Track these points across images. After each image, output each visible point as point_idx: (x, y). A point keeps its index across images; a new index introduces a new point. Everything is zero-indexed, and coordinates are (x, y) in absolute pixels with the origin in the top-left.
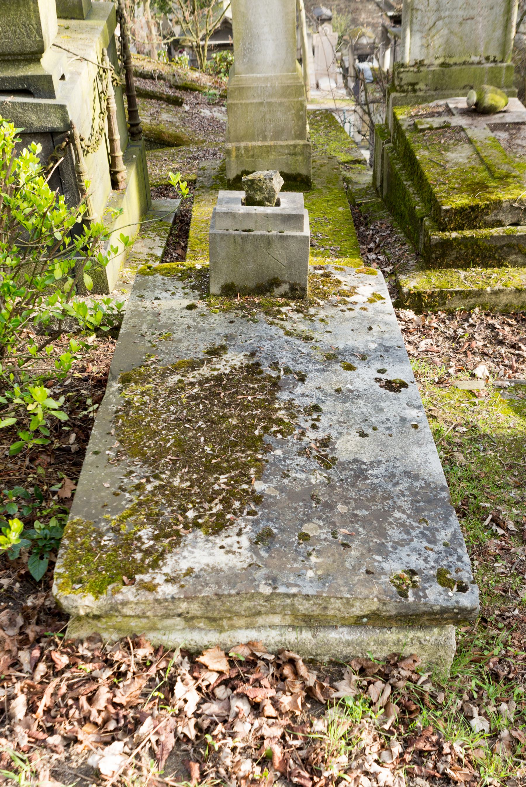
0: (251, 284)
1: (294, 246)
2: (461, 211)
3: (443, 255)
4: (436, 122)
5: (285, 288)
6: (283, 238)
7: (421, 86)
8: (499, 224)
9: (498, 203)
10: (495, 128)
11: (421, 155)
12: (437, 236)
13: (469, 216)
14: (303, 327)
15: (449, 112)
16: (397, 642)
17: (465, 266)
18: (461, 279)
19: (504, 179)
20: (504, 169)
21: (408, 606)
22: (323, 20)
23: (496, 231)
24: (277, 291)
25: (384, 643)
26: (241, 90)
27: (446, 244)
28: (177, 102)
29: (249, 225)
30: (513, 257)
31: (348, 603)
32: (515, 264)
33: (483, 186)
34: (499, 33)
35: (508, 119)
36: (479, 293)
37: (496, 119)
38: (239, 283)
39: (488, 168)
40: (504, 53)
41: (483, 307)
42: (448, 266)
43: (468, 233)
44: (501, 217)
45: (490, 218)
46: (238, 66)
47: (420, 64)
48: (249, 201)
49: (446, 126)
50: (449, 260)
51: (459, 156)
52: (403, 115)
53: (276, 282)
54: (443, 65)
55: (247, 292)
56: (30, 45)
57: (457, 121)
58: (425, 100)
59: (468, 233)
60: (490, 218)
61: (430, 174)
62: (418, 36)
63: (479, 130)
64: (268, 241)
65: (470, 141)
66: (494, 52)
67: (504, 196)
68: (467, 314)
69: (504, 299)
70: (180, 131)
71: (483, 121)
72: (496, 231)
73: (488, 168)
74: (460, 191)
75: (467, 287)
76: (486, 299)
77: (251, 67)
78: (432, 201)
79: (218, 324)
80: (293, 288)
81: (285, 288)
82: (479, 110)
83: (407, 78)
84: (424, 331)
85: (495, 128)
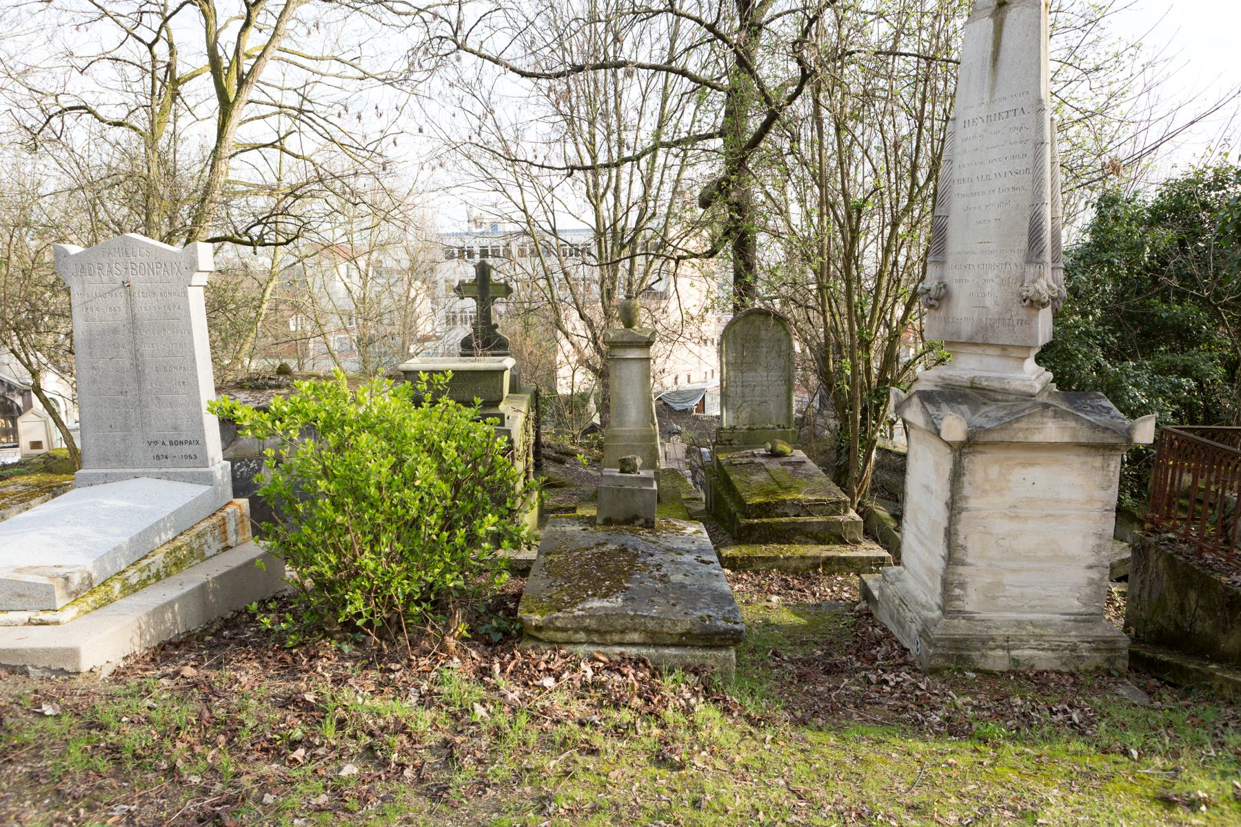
0: (621, 518)
1: (647, 496)
2: (759, 505)
3: (750, 535)
4: (745, 461)
5: (642, 521)
6: (641, 490)
7: (735, 441)
8: (786, 515)
9: (784, 501)
10: (784, 464)
11: (734, 477)
12: (744, 521)
13: (765, 509)
14: (654, 539)
15: (754, 455)
16: (702, 657)
17: (765, 543)
18: (762, 550)
19: (787, 489)
20: (788, 484)
21: (706, 627)
22: (672, 433)
23: (784, 520)
24: (637, 523)
25: (695, 657)
26: (614, 437)
27: (751, 527)
28: (562, 462)
29: (622, 482)
30: (798, 537)
31: (674, 624)
32: (800, 542)
33: (774, 492)
34: (784, 411)
35: (793, 459)
36: (776, 558)
37: (785, 459)
38: (614, 517)
39: (778, 484)
40: (789, 422)
41: (779, 568)
42: (754, 543)
43: (765, 520)
44: (787, 510)
45: (779, 511)
46: (613, 423)
47: (733, 428)
48: (622, 471)
49: (752, 463)
50: (753, 538)
51: (760, 478)
52: (722, 457)
53: (636, 518)
54: (749, 429)
55: (619, 523)
56: (495, 397)
57: (758, 460)
58: (738, 450)
59: (765, 520)
60: (779, 511)
61: (739, 487)
62: (731, 413)
63: (774, 465)
64: (632, 492)
65: (767, 470)
66: (781, 423)
67: (788, 497)
68: (768, 571)
69: (793, 564)
70: (563, 479)
71: (776, 461)
72: (784, 520)
73: (778, 484)
74: (758, 495)
75: (767, 554)
76: (781, 563)
77: (621, 423)
78: (741, 502)
79: (601, 535)
80: (647, 521)
81: (642, 521)
82: (774, 454)
83: (725, 436)
84: (737, 580)
85: (784, 464)
